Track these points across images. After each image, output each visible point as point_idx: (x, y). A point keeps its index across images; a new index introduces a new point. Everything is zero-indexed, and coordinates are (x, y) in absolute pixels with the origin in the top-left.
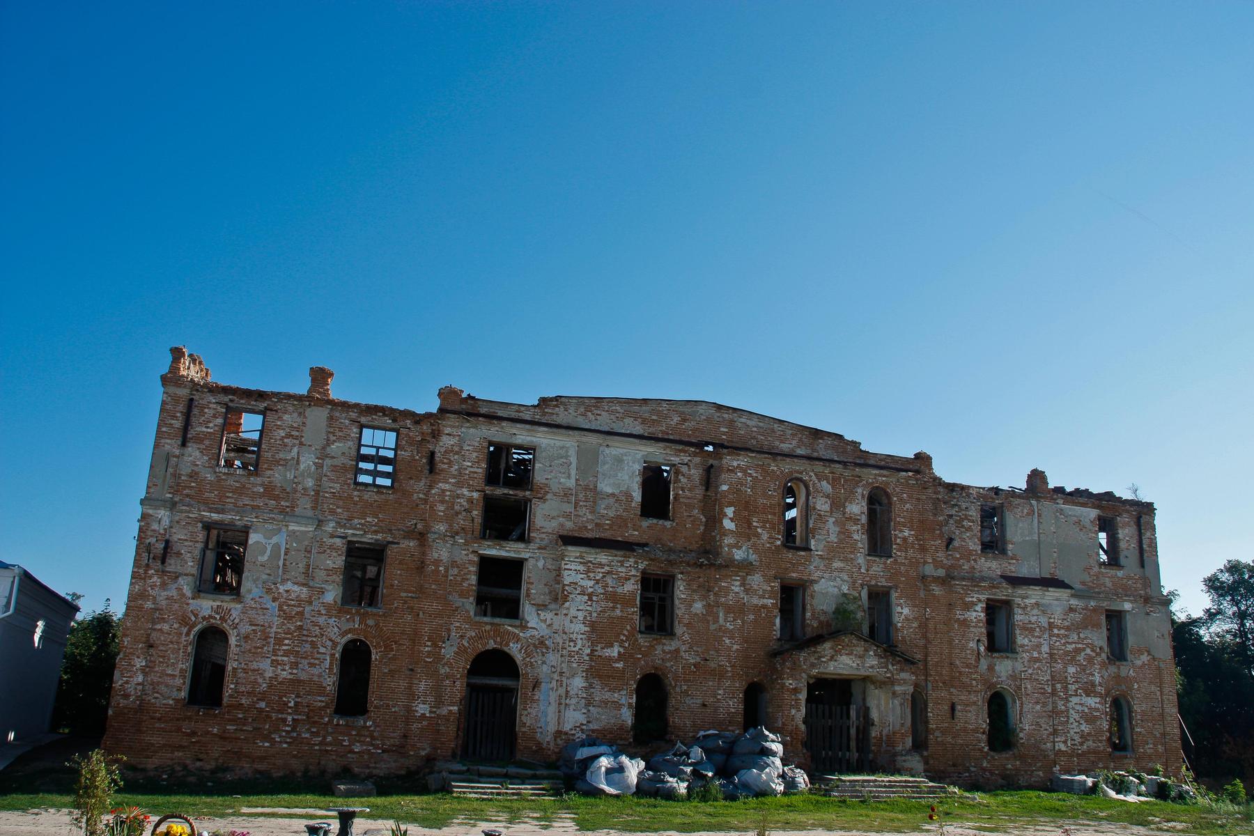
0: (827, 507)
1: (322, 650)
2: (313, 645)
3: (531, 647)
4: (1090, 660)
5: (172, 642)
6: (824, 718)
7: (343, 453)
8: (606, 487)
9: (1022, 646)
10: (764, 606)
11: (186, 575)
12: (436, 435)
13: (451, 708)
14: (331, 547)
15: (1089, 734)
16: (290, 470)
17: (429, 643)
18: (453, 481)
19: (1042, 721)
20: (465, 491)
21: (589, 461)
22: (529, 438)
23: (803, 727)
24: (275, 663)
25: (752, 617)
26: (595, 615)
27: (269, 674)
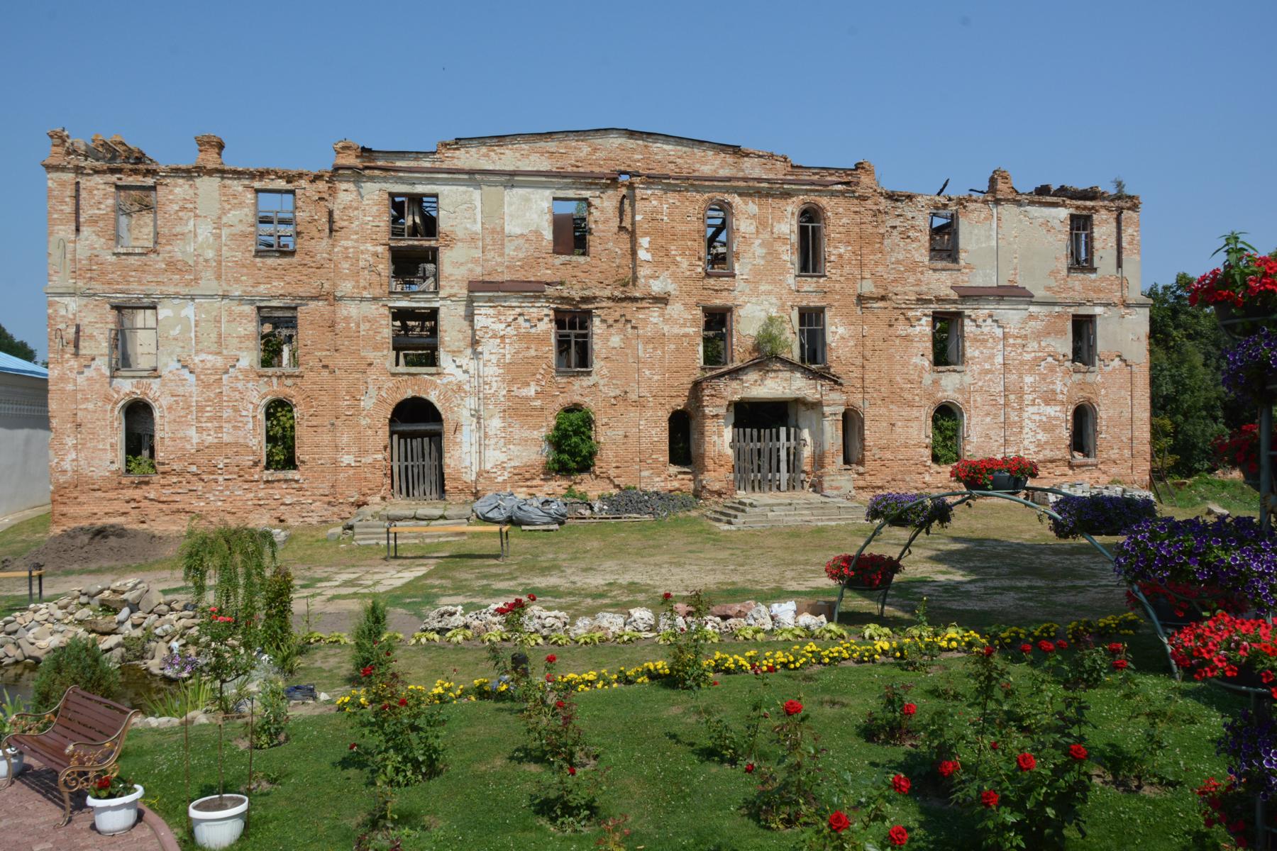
0: (752, 229)
1: (244, 413)
2: (236, 410)
3: (450, 393)
4: (1052, 370)
5: (98, 419)
6: (752, 441)
7: (241, 221)
8: (512, 228)
9: (972, 358)
10: (685, 335)
11: (102, 355)
12: (333, 191)
13: (376, 456)
14: (241, 315)
15: (1046, 443)
16: (189, 244)
17: (347, 398)
18: (355, 237)
19: (992, 433)
20: (370, 247)
21: (493, 212)
22: (429, 187)
23: (730, 452)
24: (200, 430)
25: (673, 346)
26: (508, 356)
27: (195, 441)
